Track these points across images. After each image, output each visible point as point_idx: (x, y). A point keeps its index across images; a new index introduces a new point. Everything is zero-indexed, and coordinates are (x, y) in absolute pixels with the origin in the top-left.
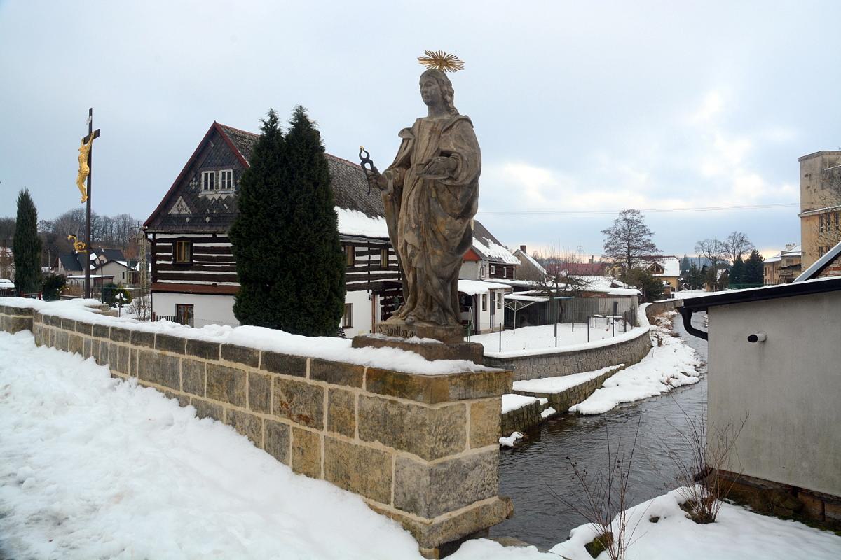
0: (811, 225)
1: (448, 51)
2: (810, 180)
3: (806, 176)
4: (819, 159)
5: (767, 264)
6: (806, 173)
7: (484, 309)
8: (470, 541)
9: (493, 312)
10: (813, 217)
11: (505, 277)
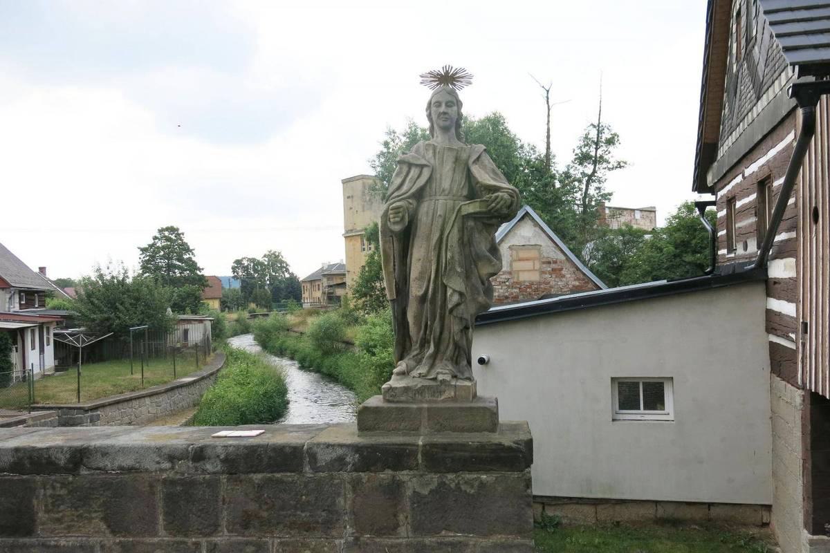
0: (353, 245)
1: (456, 65)
2: (352, 201)
3: (349, 197)
4: (361, 181)
5: (303, 282)
6: (348, 195)
7: (33, 348)
8: (777, 260)
9: (42, 350)
10: (357, 237)
11: (36, 306)
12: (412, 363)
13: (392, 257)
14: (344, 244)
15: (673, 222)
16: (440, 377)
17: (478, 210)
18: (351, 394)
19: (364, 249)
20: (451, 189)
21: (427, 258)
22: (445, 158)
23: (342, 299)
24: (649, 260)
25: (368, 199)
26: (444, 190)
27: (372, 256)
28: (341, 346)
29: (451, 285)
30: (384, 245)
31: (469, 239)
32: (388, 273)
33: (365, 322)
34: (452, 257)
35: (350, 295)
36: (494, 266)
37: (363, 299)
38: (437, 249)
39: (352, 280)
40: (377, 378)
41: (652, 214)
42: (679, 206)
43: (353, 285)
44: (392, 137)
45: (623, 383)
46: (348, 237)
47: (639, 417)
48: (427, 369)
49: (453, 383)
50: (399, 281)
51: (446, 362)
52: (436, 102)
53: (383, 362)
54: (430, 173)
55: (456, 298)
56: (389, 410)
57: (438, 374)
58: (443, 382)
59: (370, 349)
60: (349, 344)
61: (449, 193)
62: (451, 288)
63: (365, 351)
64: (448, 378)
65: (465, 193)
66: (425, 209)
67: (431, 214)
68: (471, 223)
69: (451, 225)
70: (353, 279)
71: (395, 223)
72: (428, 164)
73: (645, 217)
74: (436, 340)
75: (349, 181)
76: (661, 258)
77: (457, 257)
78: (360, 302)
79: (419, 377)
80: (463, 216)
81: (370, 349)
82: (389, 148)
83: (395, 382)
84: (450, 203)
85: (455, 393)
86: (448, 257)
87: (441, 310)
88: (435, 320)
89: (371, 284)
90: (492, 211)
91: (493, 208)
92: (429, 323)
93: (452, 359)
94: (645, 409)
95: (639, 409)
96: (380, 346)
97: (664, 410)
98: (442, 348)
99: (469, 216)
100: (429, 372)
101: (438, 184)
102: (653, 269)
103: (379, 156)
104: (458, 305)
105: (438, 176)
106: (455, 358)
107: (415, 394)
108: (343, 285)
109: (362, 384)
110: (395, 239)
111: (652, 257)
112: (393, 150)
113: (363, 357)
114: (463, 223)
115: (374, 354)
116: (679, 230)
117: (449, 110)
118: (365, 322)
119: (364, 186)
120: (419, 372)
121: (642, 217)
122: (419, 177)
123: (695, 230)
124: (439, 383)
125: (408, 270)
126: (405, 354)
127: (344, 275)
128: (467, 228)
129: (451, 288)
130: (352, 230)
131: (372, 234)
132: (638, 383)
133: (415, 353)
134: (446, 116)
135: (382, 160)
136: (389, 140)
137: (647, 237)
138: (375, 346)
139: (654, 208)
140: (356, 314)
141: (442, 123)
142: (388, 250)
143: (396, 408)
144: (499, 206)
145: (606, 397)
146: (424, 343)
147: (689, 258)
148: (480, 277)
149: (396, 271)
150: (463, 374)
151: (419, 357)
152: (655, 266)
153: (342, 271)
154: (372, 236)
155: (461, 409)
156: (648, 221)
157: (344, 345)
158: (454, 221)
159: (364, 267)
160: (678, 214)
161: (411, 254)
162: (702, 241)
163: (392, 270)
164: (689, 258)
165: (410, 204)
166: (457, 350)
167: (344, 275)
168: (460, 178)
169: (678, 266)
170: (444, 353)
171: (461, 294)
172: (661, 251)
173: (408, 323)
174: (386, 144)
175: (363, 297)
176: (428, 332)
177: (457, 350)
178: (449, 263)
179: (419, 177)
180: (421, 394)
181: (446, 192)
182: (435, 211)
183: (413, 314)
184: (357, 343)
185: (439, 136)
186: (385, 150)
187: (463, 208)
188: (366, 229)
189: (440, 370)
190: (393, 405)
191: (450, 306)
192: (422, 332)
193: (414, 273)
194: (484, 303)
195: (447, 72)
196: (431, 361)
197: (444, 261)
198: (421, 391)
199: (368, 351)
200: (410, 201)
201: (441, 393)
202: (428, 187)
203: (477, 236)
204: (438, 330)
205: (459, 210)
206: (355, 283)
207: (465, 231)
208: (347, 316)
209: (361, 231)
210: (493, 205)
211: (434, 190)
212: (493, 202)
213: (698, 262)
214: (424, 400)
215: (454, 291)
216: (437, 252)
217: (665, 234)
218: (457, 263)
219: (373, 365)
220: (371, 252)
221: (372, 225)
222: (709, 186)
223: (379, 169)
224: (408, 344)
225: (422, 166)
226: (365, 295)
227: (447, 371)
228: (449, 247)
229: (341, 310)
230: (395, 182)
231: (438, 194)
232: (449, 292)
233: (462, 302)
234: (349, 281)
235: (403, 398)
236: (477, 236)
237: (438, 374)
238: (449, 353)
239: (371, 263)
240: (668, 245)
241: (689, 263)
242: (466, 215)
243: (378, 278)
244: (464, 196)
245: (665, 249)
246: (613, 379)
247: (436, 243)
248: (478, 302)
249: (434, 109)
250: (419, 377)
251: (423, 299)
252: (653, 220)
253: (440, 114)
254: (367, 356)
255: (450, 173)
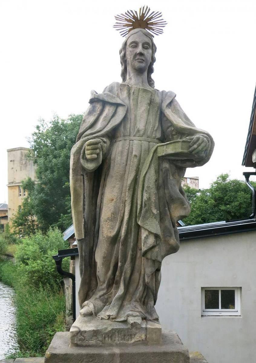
2: (14, 164)
3: (11, 161)
4: (19, 152)
10: (16, 187)
12: (99, 303)
13: (82, 197)
14: (8, 191)
15: (214, 185)
16: (131, 320)
17: (179, 150)
18: (11, 291)
19: (20, 195)
20: (145, 130)
21: (120, 198)
22: (139, 99)
23: (5, 226)
24: (199, 208)
25: (24, 163)
26: (138, 131)
27: (26, 200)
28: (4, 257)
29: (147, 227)
30: (75, 184)
31: (164, 182)
32: (77, 213)
33: (21, 242)
34: (149, 199)
35: (11, 224)
36: (185, 209)
37: (20, 227)
38: (132, 190)
39: (12, 214)
40: (29, 281)
41: (197, 181)
42: (218, 177)
43: (13, 218)
44: (42, 123)
45: (208, 291)
46: (11, 186)
47: (218, 314)
48: (117, 310)
49: (144, 326)
50: (88, 220)
51: (135, 304)
52: (132, 43)
53: (34, 269)
54: (125, 112)
55: (151, 241)
56: (80, 357)
57: (128, 316)
58: (134, 325)
59: (24, 261)
60: (10, 256)
61: (144, 134)
62: (146, 229)
63: (21, 262)
64: (138, 320)
65: (159, 135)
66: (120, 148)
67: (125, 154)
68: (166, 165)
69: (148, 165)
70: (13, 214)
71: (88, 160)
72: (123, 103)
73: (193, 182)
74: (126, 282)
75: (12, 151)
76: (207, 207)
77: (153, 198)
78: (17, 229)
79: (109, 319)
80: (159, 157)
81: (24, 261)
82: (40, 130)
83: (79, 324)
84: (145, 144)
85: (146, 336)
86: (145, 198)
87: (132, 251)
88: (125, 261)
89: (25, 218)
90: (193, 153)
91: (195, 149)
92: (119, 264)
93: (140, 301)
94: (222, 308)
95: (218, 308)
96: (32, 259)
97: (234, 308)
98: (131, 290)
99: (163, 158)
100: (118, 313)
101: (132, 125)
102: (202, 213)
103: (33, 135)
104: (153, 247)
105: (133, 117)
106: (143, 299)
107: (105, 338)
108: (6, 217)
109: (19, 284)
110: (85, 178)
111: (201, 206)
112: (42, 131)
113: (19, 266)
114: (159, 165)
115: (27, 264)
116: (217, 191)
117: (145, 52)
118: (21, 242)
119: (22, 154)
120: (108, 313)
121: (191, 183)
122: (113, 116)
123: (227, 191)
124: (129, 326)
125: (98, 210)
126: (91, 293)
127: (7, 211)
128: (161, 170)
129: (146, 229)
130: (12, 183)
131: (27, 185)
132: (218, 291)
133: (101, 293)
134: (142, 58)
135: (35, 137)
136: (40, 125)
137: (199, 194)
138: (28, 259)
139: (198, 177)
140: (15, 236)
141: (137, 64)
142: (78, 188)
143: (87, 355)
144: (200, 148)
145: (199, 300)
146: (113, 283)
147: (223, 207)
148: (171, 218)
149: (86, 210)
150: (151, 315)
151: (106, 296)
152: (203, 212)
153: (5, 209)
154: (29, 186)
155: (155, 354)
156: (194, 185)
157: (6, 257)
158: (151, 162)
159: (20, 206)
160: (217, 181)
161: (103, 194)
162: (230, 198)
163: (81, 209)
164: (223, 207)
165: (104, 142)
166: (146, 291)
167: (7, 211)
168: (154, 121)
169: (216, 212)
170: (134, 294)
171: (156, 236)
172: (207, 203)
173: (95, 263)
174: (38, 127)
175: (20, 226)
176: (118, 273)
177: (146, 291)
178: (145, 205)
179: (113, 116)
180: (111, 337)
181: (141, 133)
182: (129, 152)
183: (102, 255)
184: (16, 256)
185: (133, 78)
186: (37, 131)
187: (159, 149)
188: (23, 182)
189: (130, 313)
190: (83, 351)
191: (144, 249)
192: (110, 273)
193: (106, 213)
194: (174, 245)
195: (143, 16)
196: (120, 303)
197: (139, 202)
198: (111, 334)
199: (24, 262)
200: (105, 139)
201: (131, 336)
202: (122, 126)
203: (171, 178)
204: (129, 272)
205: (156, 151)
206: (14, 217)
207: (161, 172)
208: (8, 238)
209: (19, 183)
210: (195, 146)
211: (128, 130)
212: (195, 143)
213: (228, 210)
214: (114, 344)
215: (150, 233)
216: (131, 193)
217: (209, 193)
218: (153, 205)
219: (26, 272)
220: (26, 196)
221: (27, 179)
222: (253, 162)
223: (33, 143)
224: (94, 282)
225: (117, 105)
226: (21, 224)
227: (138, 314)
228: (145, 188)
229: (4, 234)
230: (88, 121)
231: (132, 135)
232: (144, 234)
233: (157, 245)
234: (10, 215)
235: (93, 342)
236: (171, 178)
237: (128, 316)
238: (138, 294)
239: (25, 204)
240: (211, 199)
241: (223, 210)
242: (163, 156)
243: (30, 214)
244: (158, 139)
245: (209, 202)
246: (202, 288)
247: (131, 183)
248: (169, 245)
249: (129, 49)
250: (109, 319)
251: (114, 240)
252: (197, 185)
253: (136, 55)
254: (23, 265)
255: (145, 115)
